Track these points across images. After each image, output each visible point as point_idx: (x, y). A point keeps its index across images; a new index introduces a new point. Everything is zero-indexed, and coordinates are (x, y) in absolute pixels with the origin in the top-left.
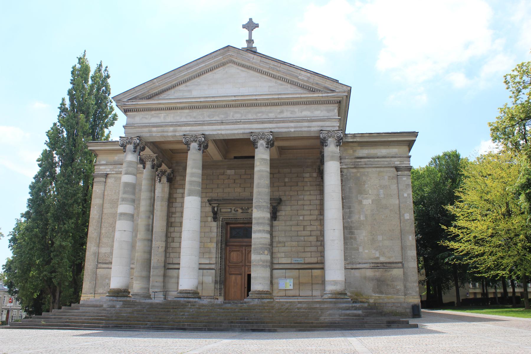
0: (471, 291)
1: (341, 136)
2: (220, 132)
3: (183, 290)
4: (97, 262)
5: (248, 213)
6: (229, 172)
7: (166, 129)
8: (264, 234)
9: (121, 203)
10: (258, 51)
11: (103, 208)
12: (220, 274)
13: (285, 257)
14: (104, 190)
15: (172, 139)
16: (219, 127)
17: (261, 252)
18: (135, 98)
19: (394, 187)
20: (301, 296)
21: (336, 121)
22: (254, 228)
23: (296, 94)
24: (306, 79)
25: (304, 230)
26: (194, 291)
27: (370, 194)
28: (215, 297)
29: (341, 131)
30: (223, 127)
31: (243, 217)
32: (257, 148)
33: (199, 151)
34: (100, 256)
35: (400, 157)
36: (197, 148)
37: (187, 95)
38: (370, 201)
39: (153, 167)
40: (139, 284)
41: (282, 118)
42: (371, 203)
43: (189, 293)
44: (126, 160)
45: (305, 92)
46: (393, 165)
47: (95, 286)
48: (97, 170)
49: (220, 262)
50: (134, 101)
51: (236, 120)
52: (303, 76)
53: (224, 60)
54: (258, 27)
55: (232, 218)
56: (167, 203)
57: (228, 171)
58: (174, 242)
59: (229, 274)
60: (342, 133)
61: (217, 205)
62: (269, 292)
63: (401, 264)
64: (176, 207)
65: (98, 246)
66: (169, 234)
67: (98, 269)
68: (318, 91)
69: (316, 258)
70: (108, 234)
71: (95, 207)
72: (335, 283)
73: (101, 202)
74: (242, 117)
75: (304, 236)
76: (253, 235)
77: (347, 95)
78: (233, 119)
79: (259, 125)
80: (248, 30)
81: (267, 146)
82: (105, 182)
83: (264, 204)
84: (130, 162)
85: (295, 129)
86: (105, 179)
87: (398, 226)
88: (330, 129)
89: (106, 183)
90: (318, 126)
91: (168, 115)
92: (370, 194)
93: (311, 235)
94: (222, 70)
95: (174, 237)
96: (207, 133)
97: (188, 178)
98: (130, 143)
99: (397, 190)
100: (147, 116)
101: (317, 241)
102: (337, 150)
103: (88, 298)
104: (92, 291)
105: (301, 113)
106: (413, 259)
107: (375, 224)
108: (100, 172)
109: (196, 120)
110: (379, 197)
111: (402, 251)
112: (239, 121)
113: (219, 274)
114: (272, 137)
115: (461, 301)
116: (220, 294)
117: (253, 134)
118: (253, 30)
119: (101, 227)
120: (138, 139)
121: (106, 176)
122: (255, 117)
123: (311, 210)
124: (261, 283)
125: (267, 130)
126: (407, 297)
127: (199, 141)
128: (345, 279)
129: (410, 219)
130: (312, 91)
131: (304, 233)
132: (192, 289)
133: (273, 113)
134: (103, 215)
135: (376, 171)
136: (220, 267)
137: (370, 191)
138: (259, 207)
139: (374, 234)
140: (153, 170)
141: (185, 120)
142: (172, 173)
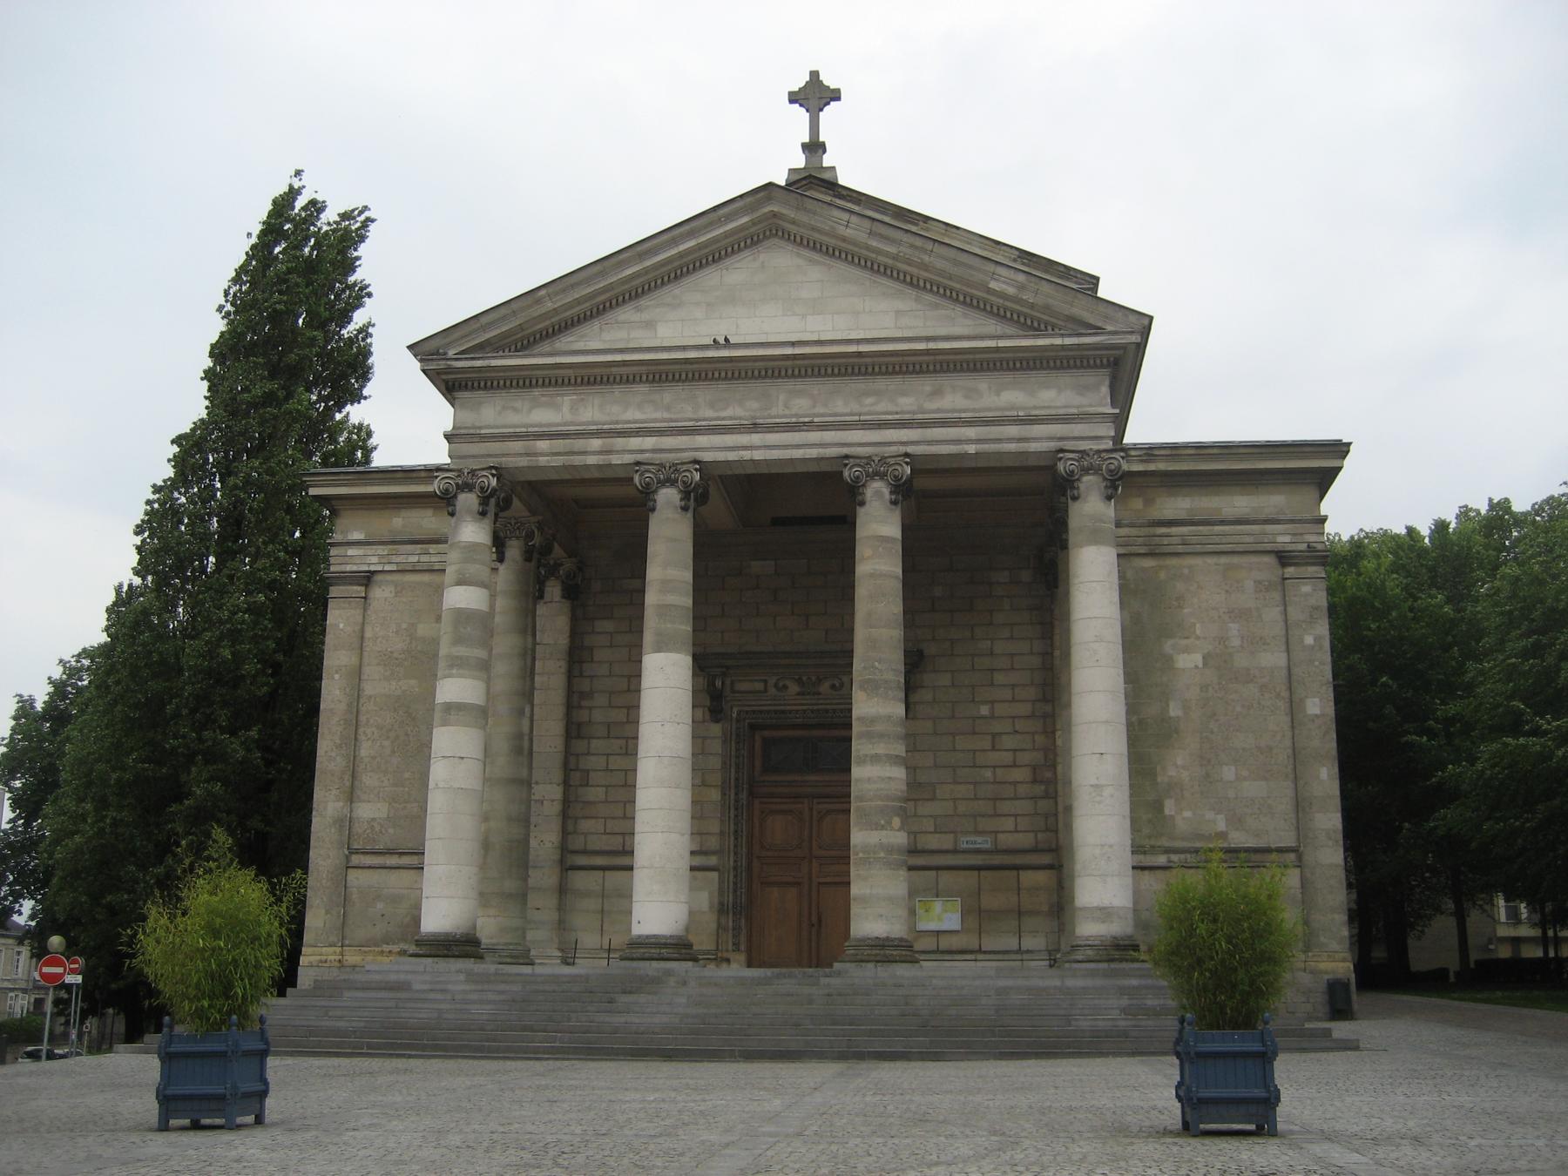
0: (1503, 932)
1: (1120, 467)
2: (747, 455)
3: (647, 937)
4: (348, 848)
5: (820, 694)
6: (756, 566)
7: (579, 444)
8: (888, 768)
9: (447, 672)
10: (841, 181)
11: (360, 680)
12: (735, 884)
13: (935, 832)
14: (363, 624)
15: (597, 475)
16: (744, 439)
17: (883, 822)
18: (480, 347)
19: (1273, 614)
20: (985, 952)
21: (1106, 420)
22: (858, 747)
23: (982, 338)
24: (1011, 291)
25: (993, 749)
26: (680, 937)
27: (1198, 638)
28: (719, 955)
29: (1122, 454)
30: (756, 439)
31: (805, 707)
32: (862, 504)
33: (684, 513)
34: (357, 829)
35: (1292, 521)
36: (678, 503)
37: (642, 338)
38: (1197, 659)
39: (528, 555)
40: (495, 916)
41: (938, 411)
42: (1201, 665)
43: (665, 945)
44: (456, 541)
45: (1010, 330)
46: (1269, 547)
47: (344, 923)
48: (340, 560)
49: (735, 846)
50: (477, 356)
51: (796, 415)
52: (1003, 284)
53: (756, 228)
54: (838, 99)
55: (768, 712)
56: (563, 664)
57: (753, 563)
58: (587, 785)
59: (762, 883)
60: (1123, 458)
61: (724, 670)
62: (906, 941)
63: (1296, 854)
64: (592, 677)
65: (351, 797)
66: (572, 760)
67: (350, 870)
68: (1049, 328)
69: (1031, 835)
70: (379, 759)
71: (337, 677)
72: (1105, 913)
73: (354, 660)
74: (814, 407)
75: (994, 767)
76: (856, 771)
77: (1139, 340)
78: (787, 412)
79: (868, 432)
80: (807, 111)
81: (893, 497)
82: (365, 598)
83: (890, 676)
84: (473, 547)
85: (978, 446)
86: (363, 588)
87: (1284, 736)
88: (1087, 448)
89: (368, 601)
90: (1051, 439)
91: (583, 400)
92: (1198, 638)
93: (1015, 762)
94: (750, 258)
95: (588, 771)
96: (707, 457)
97: (651, 598)
98: (467, 487)
99: (1283, 623)
100: (518, 404)
101: (1034, 781)
102: (1109, 511)
103: (324, 958)
104: (333, 939)
105: (998, 395)
106: (1330, 839)
107: (1215, 730)
108: (348, 568)
109: (673, 416)
110: (1226, 647)
111: (1298, 812)
112: (806, 420)
113: (731, 884)
114: (909, 472)
115: (1472, 965)
116: (736, 945)
117: (851, 460)
118: (821, 110)
119: (356, 739)
120: (493, 475)
121: (367, 579)
122: (855, 407)
123: (1013, 686)
124: (881, 916)
125: (893, 450)
126: (1314, 956)
127: (684, 482)
128: (1136, 903)
129: (1323, 715)
130: (1032, 328)
131: (994, 757)
132: (674, 933)
133: (907, 397)
134: (362, 701)
135: (1216, 564)
136: (735, 861)
137: (1198, 625)
138: (873, 687)
139: (1209, 761)
140: (527, 563)
141: (638, 415)
142: (580, 569)
